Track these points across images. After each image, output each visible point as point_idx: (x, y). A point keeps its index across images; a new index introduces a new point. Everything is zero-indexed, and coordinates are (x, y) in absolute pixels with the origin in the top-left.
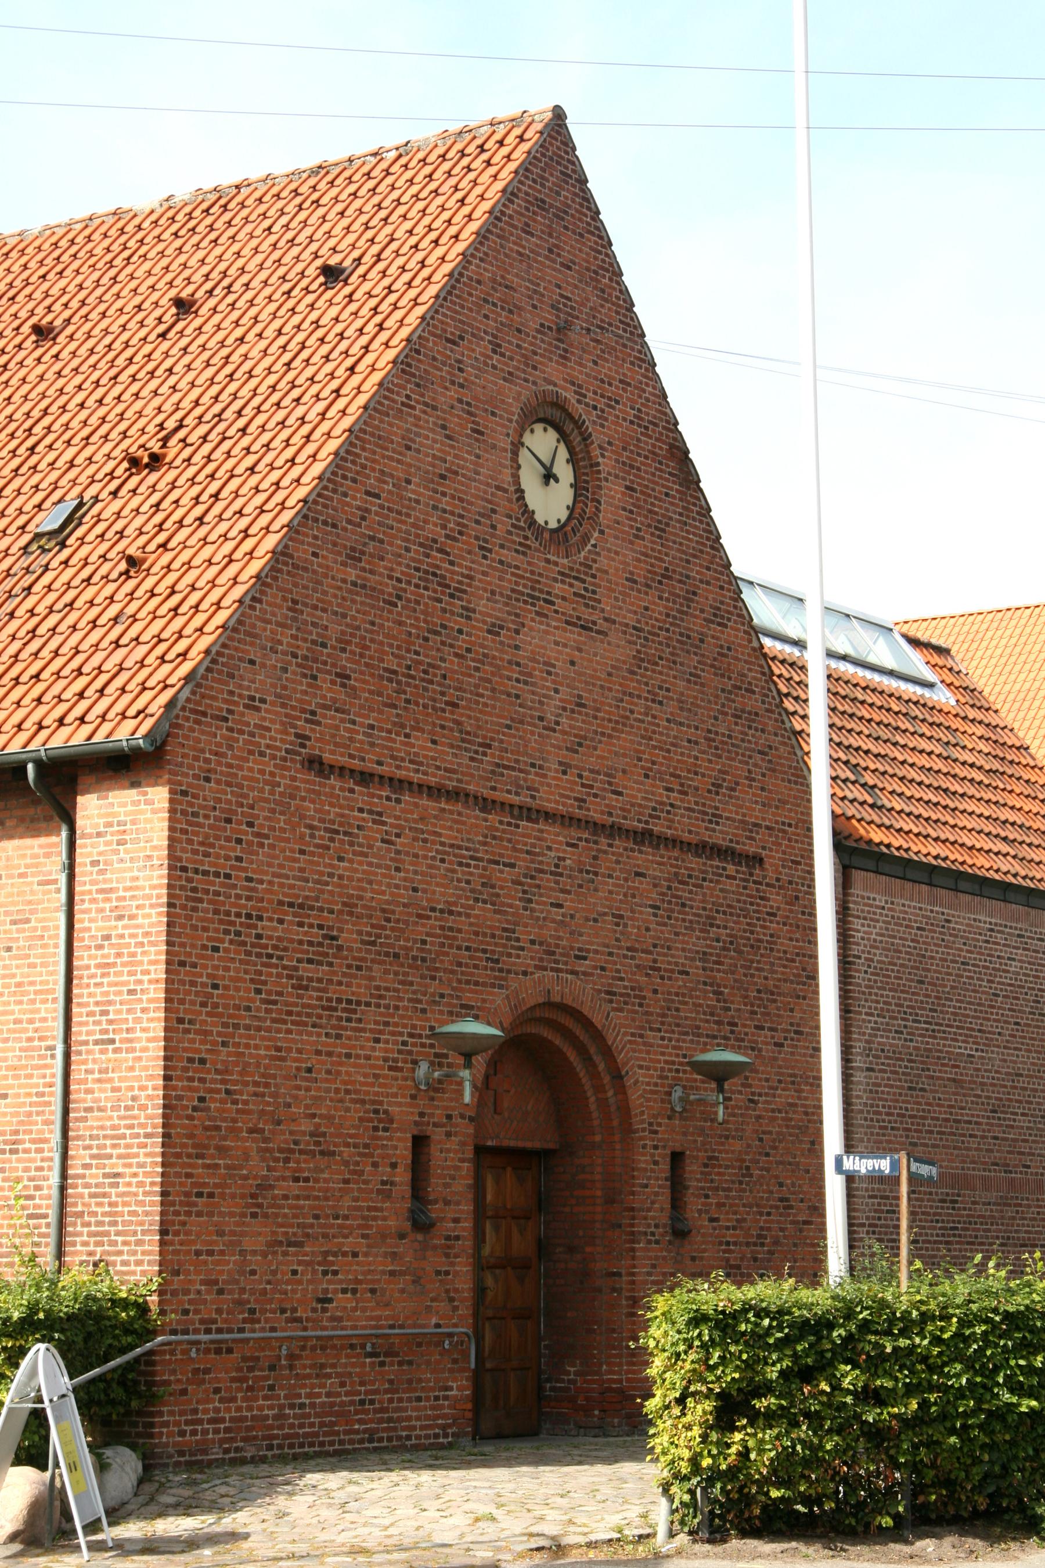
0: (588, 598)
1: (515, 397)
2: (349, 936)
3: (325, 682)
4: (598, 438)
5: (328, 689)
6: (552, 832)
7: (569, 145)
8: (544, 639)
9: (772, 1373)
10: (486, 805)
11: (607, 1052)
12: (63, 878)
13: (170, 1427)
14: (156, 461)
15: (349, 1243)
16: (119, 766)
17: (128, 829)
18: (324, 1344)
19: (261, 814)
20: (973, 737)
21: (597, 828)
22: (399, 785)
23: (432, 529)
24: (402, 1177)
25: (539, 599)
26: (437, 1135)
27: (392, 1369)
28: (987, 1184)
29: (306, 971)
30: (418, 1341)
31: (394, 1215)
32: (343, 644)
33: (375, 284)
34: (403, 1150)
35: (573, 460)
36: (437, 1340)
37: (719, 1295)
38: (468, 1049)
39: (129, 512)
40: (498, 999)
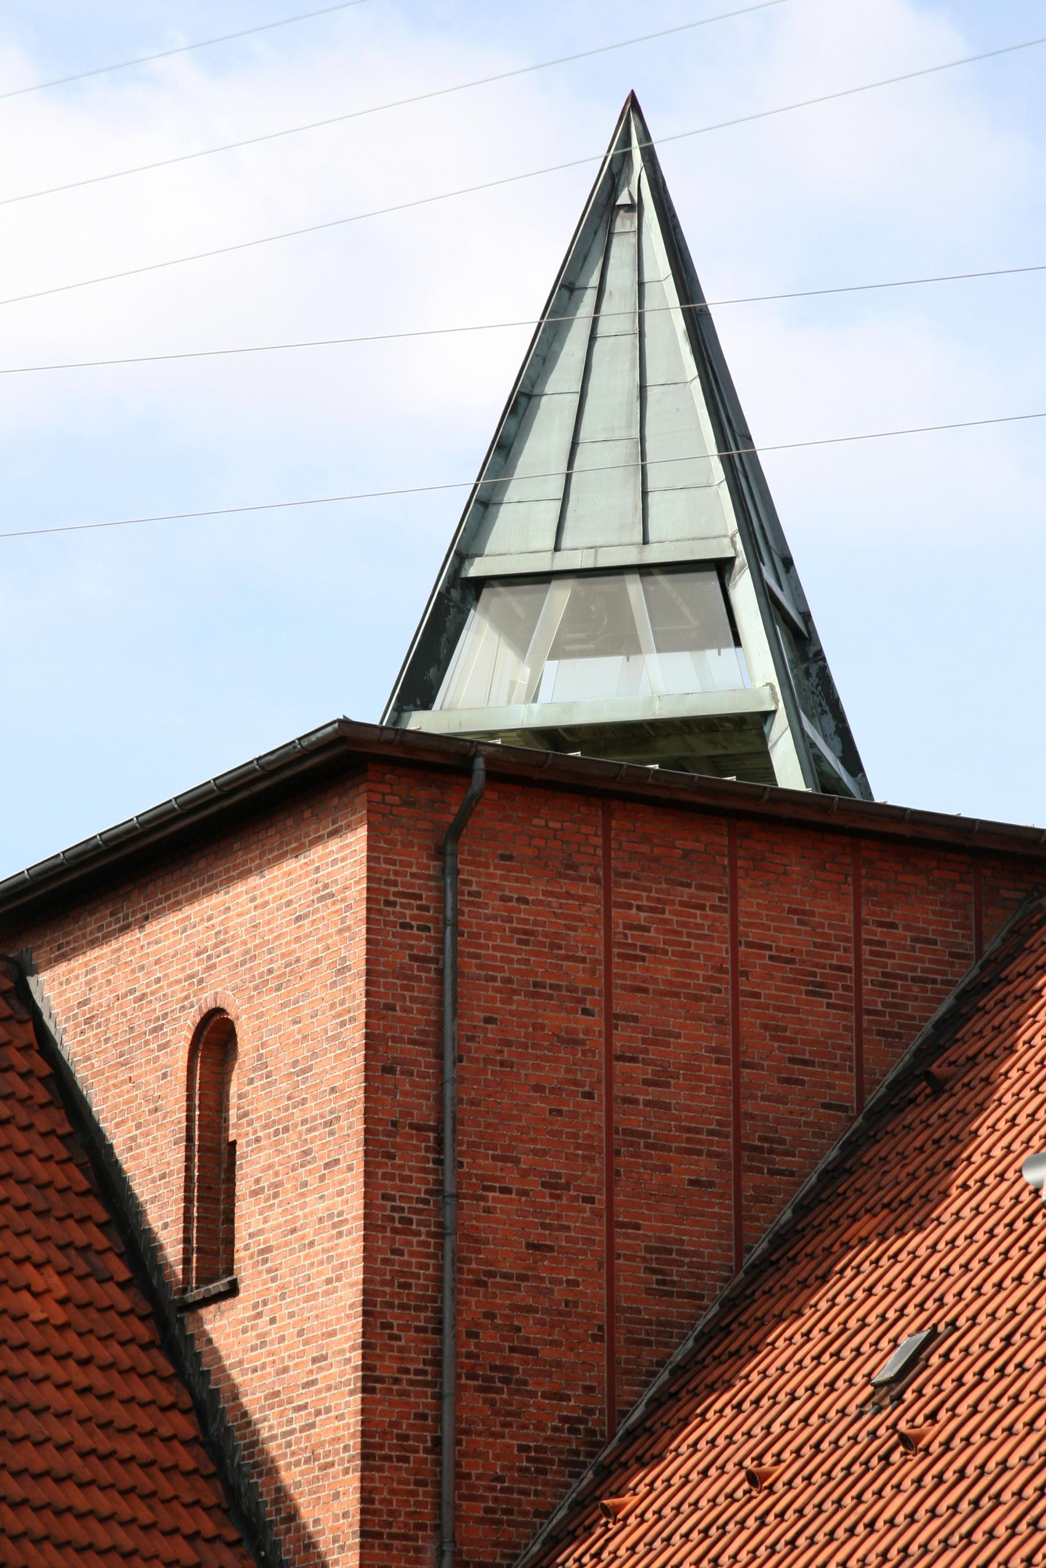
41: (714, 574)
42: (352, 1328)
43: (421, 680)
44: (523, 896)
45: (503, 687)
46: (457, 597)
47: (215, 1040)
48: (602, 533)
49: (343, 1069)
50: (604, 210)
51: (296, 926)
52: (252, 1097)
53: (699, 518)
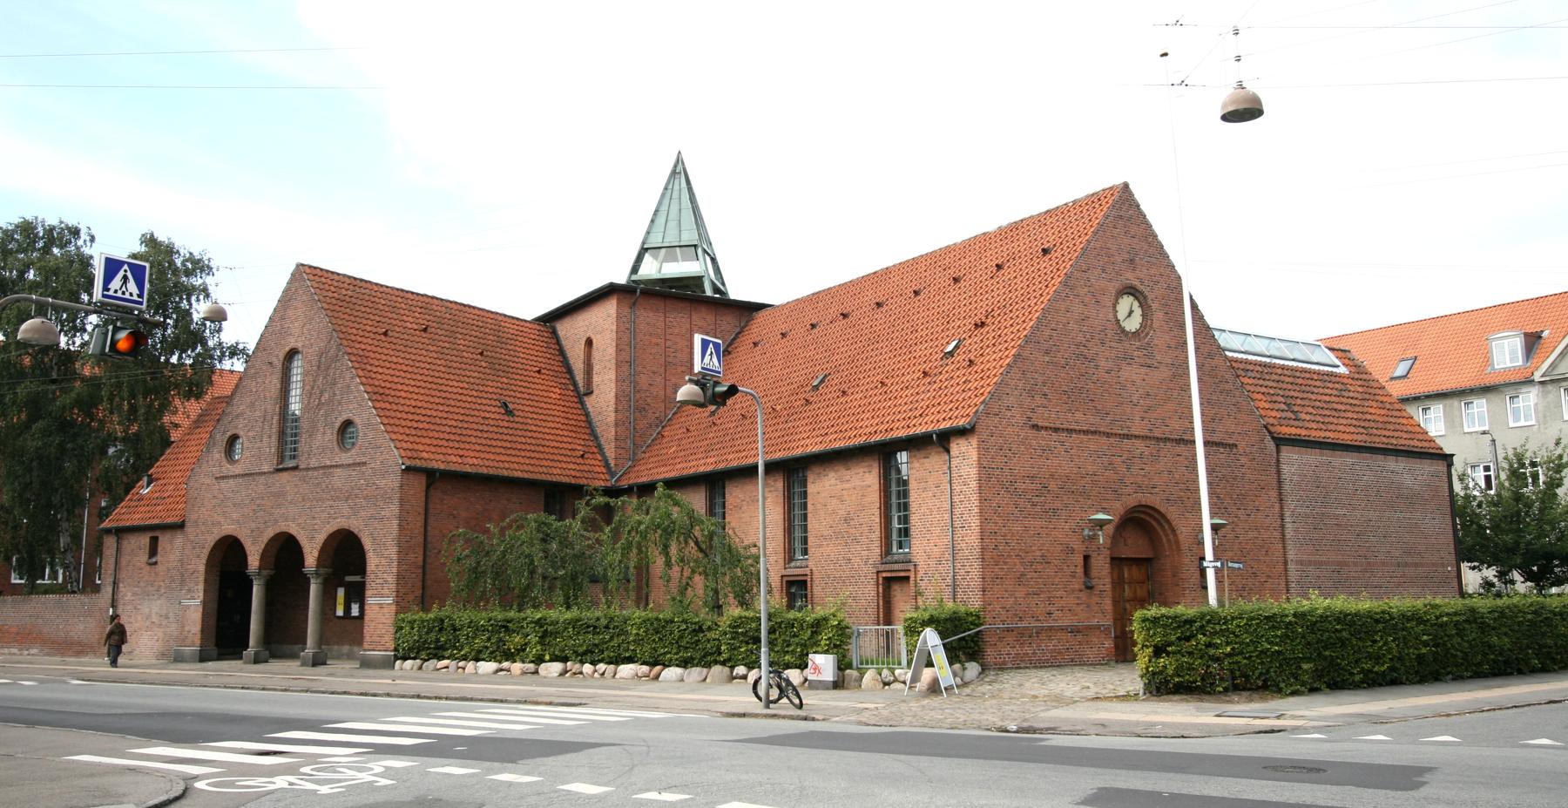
0: (1150, 356)
1: (1113, 288)
2: (1052, 486)
3: (1037, 398)
4: (1150, 296)
5: (1039, 400)
6: (1137, 442)
7: (1131, 195)
8: (1130, 373)
9: (1173, 638)
10: (1108, 435)
11: (1168, 521)
12: (429, 583)
13: (990, 654)
14: (983, 324)
15: (1058, 594)
16: (962, 432)
17: (965, 453)
18: (1051, 629)
19: (1014, 447)
20: (1356, 387)
21: (1158, 439)
22: (1070, 431)
23: (1080, 339)
24: (1080, 570)
25: (1128, 358)
26: (1094, 555)
27: (1079, 637)
28: (1355, 564)
29: (1035, 499)
30: (1089, 628)
31: (1077, 584)
32: (1044, 384)
33: (1058, 254)
34: (1080, 561)
35: (1141, 305)
36: (1098, 627)
37: (1154, 611)
38: (1101, 524)
39: (973, 343)
40: (1118, 505)
41: (423, 479)
42: (613, 401)
43: (635, 270)
44: (650, 318)
45: (651, 269)
46: (643, 251)
47: (589, 342)
48: (671, 239)
49: (612, 350)
50: (674, 173)
51: (604, 318)
52: (596, 355)
53: (689, 236)
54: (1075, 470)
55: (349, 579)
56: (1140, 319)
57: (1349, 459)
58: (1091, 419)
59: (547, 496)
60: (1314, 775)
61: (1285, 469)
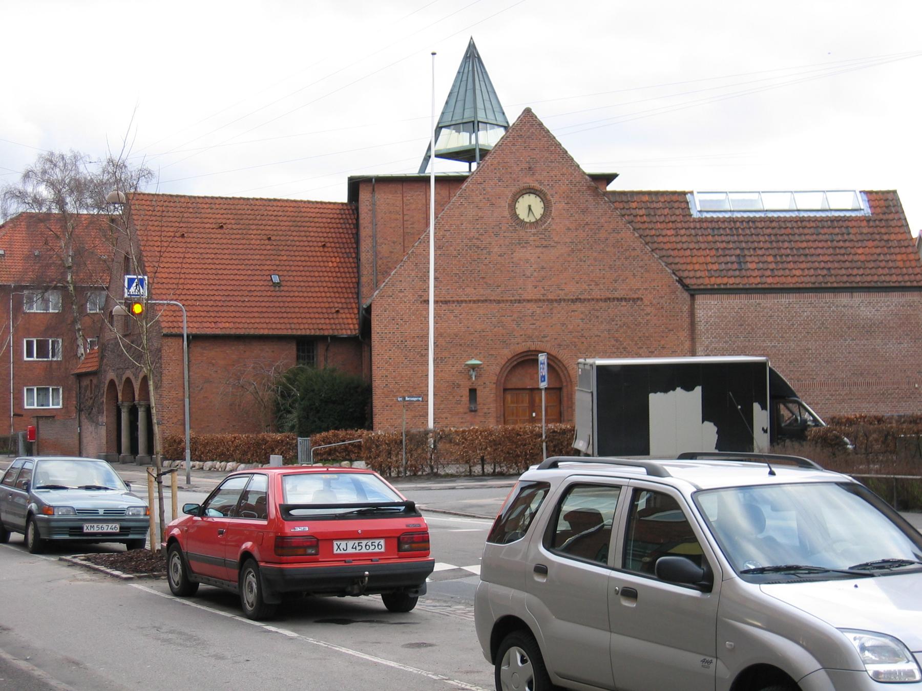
6: (529, 305)
19: (406, 317)
22: (460, 302)
34: (466, 393)
54: (463, 329)
55: (265, 523)
56: (521, 217)
57: (792, 298)
58: (482, 292)
59: (298, 345)
60: (115, 443)
61: (700, 314)
